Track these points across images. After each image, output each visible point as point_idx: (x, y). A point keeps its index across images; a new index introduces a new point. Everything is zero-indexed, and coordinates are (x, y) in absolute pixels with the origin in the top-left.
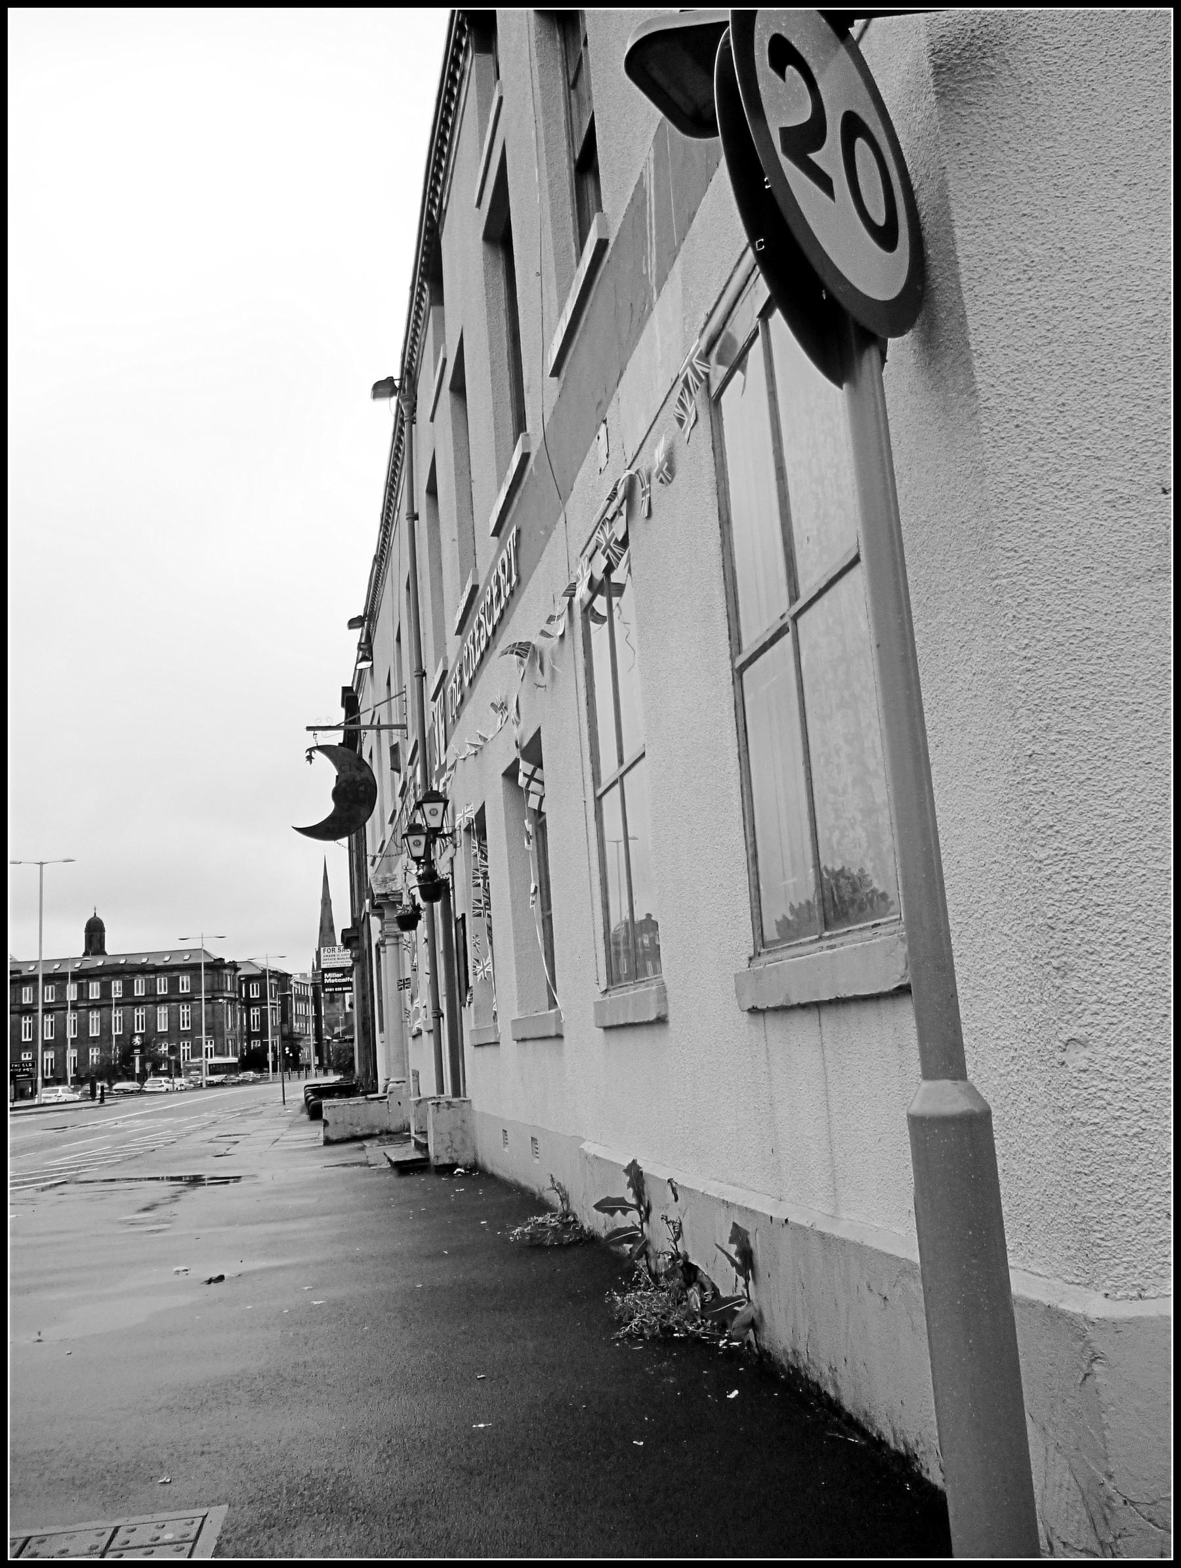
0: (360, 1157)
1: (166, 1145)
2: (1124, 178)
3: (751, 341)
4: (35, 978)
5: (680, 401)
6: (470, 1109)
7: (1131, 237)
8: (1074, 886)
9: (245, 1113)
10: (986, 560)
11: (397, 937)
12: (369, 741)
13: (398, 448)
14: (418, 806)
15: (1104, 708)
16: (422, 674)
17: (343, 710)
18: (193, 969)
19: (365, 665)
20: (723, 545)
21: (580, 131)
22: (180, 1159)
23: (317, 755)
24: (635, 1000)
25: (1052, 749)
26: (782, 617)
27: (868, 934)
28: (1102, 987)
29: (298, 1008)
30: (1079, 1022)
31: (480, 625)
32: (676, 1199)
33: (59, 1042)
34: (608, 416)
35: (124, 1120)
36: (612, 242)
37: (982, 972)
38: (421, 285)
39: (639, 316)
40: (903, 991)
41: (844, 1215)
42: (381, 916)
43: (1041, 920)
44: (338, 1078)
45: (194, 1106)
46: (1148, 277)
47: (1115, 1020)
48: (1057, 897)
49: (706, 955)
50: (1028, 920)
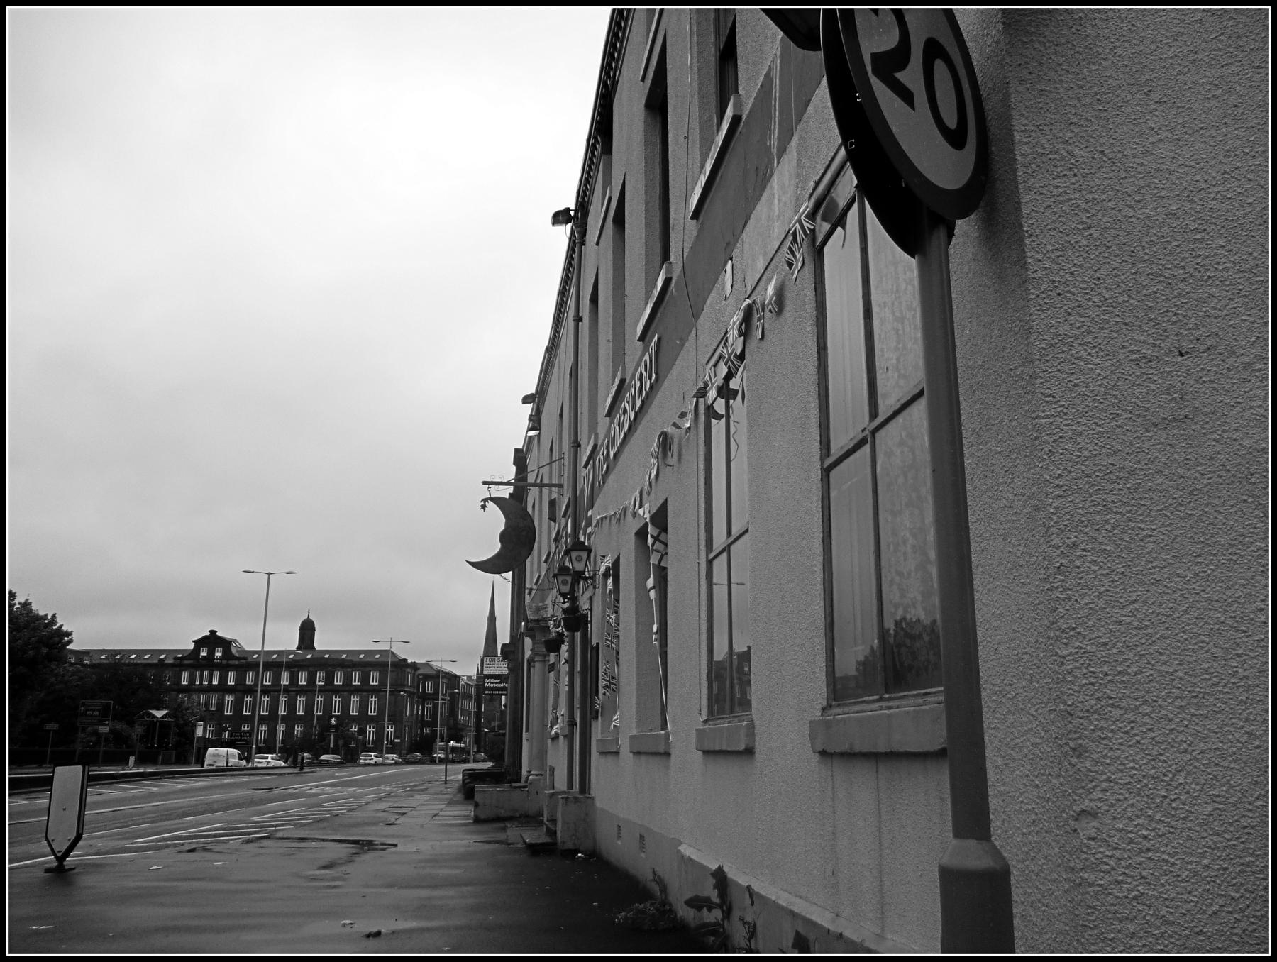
0: (501, 836)
1: (349, 811)
2: (1156, 97)
3: (849, 206)
4: (258, 665)
5: (790, 249)
6: (593, 803)
7: (1160, 145)
8: (1092, 680)
9: (413, 790)
10: (1029, 402)
11: (544, 656)
12: (533, 493)
13: (570, 263)
14: (567, 552)
15: (1124, 532)
16: (577, 445)
17: (514, 468)
18: (381, 666)
19: (532, 433)
20: (820, 365)
21: (726, 22)
22: (357, 825)
23: (490, 504)
24: (728, 730)
25: (1077, 563)
26: (863, 431)
27: (921, 701)
28: (1112, 768)
29: (464, 704)
30: (1091, 796)
31: (625, 411)
32: (752, 904)
33: (271, 720)
34: (734, 255)
35: (317, 786)
36: (744, 117)
37: (1011, 744)
38: (595, 138)
39: (763, 179)
40: (942, 753)
41: (889, 936)
42: (533, 638)
43: (1062, 707)
44: (490, 764)
45: (374, 779)
46: (1173, 178)
47: (1121, 797)
48: (1076, 688)
49: (788, 699)
50: (1051, 706)
